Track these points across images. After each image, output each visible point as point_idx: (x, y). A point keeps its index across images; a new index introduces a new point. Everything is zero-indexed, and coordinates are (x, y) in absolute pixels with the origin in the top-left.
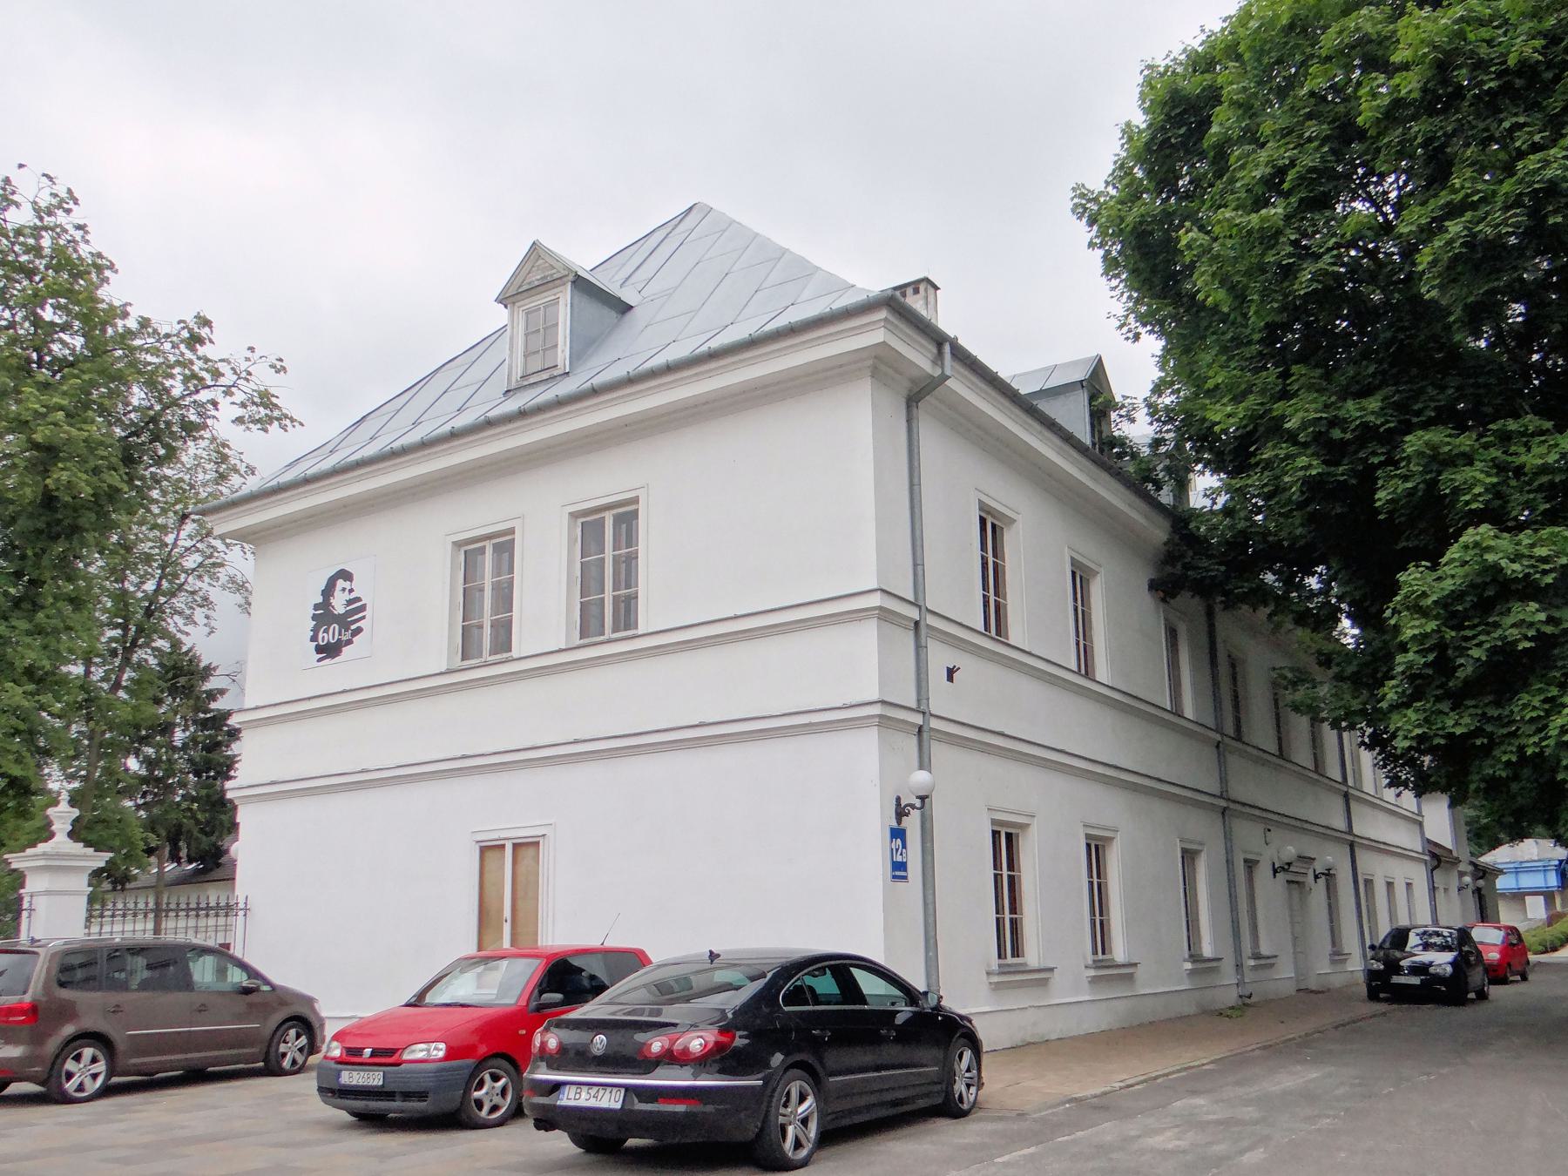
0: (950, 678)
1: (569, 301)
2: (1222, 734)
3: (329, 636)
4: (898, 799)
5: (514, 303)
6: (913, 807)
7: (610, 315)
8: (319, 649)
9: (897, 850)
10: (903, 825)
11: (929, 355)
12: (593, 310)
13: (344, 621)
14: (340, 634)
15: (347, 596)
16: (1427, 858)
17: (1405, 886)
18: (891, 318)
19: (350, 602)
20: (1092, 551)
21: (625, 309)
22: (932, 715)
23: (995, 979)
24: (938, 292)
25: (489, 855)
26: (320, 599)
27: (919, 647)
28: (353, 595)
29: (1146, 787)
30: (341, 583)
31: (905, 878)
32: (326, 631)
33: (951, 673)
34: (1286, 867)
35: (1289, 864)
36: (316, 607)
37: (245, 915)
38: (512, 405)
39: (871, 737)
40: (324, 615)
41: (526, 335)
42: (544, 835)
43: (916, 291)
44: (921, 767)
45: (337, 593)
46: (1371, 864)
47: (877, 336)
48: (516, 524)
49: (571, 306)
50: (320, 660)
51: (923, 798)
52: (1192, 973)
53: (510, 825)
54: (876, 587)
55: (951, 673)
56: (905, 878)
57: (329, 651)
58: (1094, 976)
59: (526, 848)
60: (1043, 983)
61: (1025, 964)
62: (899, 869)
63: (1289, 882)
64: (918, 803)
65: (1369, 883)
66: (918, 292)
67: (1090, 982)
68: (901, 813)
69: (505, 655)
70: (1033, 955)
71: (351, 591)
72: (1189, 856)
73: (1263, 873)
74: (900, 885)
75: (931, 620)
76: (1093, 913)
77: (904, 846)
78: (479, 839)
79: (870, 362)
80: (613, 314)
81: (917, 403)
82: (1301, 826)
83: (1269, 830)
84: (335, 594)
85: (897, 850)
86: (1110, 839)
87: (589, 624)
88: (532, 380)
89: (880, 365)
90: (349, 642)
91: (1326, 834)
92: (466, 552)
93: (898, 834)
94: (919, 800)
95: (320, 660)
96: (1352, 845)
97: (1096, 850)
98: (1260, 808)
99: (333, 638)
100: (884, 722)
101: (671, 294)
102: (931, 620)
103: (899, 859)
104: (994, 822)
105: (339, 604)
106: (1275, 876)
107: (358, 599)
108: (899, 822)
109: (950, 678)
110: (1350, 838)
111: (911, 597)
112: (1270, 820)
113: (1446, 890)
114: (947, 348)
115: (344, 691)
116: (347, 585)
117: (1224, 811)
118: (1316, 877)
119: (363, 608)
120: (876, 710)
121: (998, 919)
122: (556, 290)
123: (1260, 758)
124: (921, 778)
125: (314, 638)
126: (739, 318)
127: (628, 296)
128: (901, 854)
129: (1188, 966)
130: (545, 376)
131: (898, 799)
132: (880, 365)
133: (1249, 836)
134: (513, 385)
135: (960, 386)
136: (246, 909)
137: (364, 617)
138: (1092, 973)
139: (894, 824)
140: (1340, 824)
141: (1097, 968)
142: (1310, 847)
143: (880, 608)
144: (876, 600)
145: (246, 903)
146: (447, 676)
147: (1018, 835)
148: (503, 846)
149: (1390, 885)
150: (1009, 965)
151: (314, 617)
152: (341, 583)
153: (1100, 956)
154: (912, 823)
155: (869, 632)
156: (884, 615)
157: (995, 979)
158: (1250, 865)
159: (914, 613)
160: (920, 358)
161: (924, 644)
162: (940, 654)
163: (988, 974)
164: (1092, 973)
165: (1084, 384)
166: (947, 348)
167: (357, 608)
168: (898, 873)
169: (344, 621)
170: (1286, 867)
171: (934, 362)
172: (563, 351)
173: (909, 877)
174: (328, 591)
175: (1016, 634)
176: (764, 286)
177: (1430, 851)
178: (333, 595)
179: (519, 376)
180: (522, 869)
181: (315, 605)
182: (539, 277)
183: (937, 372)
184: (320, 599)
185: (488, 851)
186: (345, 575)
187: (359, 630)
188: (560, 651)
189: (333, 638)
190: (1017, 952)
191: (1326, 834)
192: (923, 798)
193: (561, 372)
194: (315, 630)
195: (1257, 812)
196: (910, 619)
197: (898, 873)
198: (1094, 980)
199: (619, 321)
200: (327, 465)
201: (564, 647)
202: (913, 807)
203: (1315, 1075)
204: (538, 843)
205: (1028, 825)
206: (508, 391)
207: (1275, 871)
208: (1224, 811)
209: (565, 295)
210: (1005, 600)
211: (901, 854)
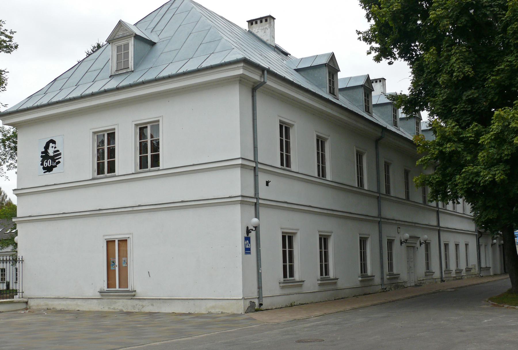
0: (267, 185)
1: (133, 44)
2: (380, 193)
3: (49, 163)
4: (248, 227)
5: (112, 42)
6: (252, 230)
7: (148, 47)
8: (44, 168)
9: (247, 244)
10: (249, 236)
11: (259, 75)
12: (142, 46)
13: (53, 158)
14: (52, 163)
15: (53, 149)
16: (476, 233)
17: (454, 246)
18: (245, 65)
19: (55, 152)
20: (324, 132)
21: (153, 44)
22: (260, 199)
23: (282, 285)
24: (275, 20)
25: (110, 244)
26: (44, 150)
27: (256, 176)
28: (56, 149)
29: (345, 216)
30: (51, 145)
31: (250, 253)
32: (47, 162)
33: (267, 183)
34: (405, 241)
35: (406, 240)
36: (42, 153)
37: (22, 263)
38: (113, 84)
39: (238, 207)
40: (45, 156)
41: (117, 63)
42: (129, 237)
43: (266, 21)
44: (256, 217)
45: (50, 148)
46: (445, 237)
47: (240, 72)
48: (116, 127)
49: (134, 46)
50: (44, 172)
51: (255, 227)
52: (361, 281)
53: (117, 234)
54: (239, 157)
55: (267, 183)
56: (250, 253)
57: (49, 169)
58: (320, 283)
59: (123, 242)
60: (301, 286)
61: (294, 280)
62: (247, 250)
63: (407, 246)
64: (254, 229)
65: (446, 245)
66: (267, 21)
67: (319, 285)
68: (248, 231)
69: (113, 174)
70: (297, 276)
71: (55, 147)
72: (363, 241)
73: (396, 246)
74: (248, 255)
75: (260, 166)
76: (321, 261)
77: (250, 243)
78: (106, 238)
79: (239, 79)
80: (149, 46)
81: (256, 90)
82: (414, 225)
83: (399, 228)
84: (49, 148)
85: (247, 244)
86: (329, 236)
87: (143, 164)
88: (120, 72)
89: (241, 80)
90: (56, 166)
91: (428, 228)
92: (97, 135)
93: (247, 239)
94: (254, 228)
95: (44, 172)
96: (439, 231)
97: (324, 240)
98: (395, 220)
99: (49, 165)
100: (242, 203)
101: (170, 40)
102: (260, 166)
103: (248, 247)
104: (283, 233)
105: (51, 152)
106: (401, 245)
107: (58, 151)
108: (248, 235)
109: (267, 185)
110: (438, 228)
111: (252, 159)
112: (399, 224)
113: (486, 246)
114: (266, 72)
115: (55, 184)
116: (54, 145)
117: (379, 222)
118: (421, 244)
119: (60, 154)
120: (240, 199)
121: (320, 251)
122: (128, 39)
123: (398, 201)
124: (255, 220)
125: (42, 164)
126: (195, 56)
127: (154, 39)
128: (248, 245)
129: (360, 279)
130: (124, 71)
131: (248, 227)
132: (241, 80)
133: (389, 232)
134: (113, 74)
135: (271, 83)
136: (22, 261)
137: (60, 158)
138: (319, 282)
139: (246, 235)
140: (435, 223)
141: (321, 280)
142: (418, 233)
143: (241, 164)
144: (240, 162)
145: (22, 259)
146: (92, 181)
147: (293, 236)
148: (114, 241)
149: (457, 245)
150: (288, 280)
151: (42, 157)
152: (51, 145)
153: (324, 276)
154: (253, 235)
155: (238, 172)
156: (242, 166)
157: (282, 285)
158: (390, 242)
159: (254, 165)
160: (256, 76)
161: (257, 175)
162: (262, 178)
163: (280, 283)
164: (319, 282)
165: (326, 65)
166: (266, 72)
167: (57, 154)
168: (247, 252)
169: (53, 158)
170: (405, 241)
171: (261, 77)
172: (131, 62)
173: (251, 253)
174: (47, 147)
175: (294, 167)
176: (203, 42)
177: (478, 231)
178: (48, 149)
179: (115, 70)
180: (122, 248)
181: (42, 152)
182: (121, 33)
183: (262, 80)
184: (44, 150)
185: (110, 243)
186: (53, 142)
187: (59, 162)
188: (133, 174)
189: (49, 165)
190: (292, 275)
191: (428, 228)
192: (255, 227)
193: (130, 70)
194: (42, 162)
195: (394, 222)
196: (253, 166)
197: (247, 252)
198: (320, 285)
199: (151, 49)
200: (45, 101)
201: (134, 172)
202: (252, 230)
203: (23, 312)
204: (127, 240)
205: (296, 233)
206: (111, 76)
207: (401, 243)
208: (379, 222)
209: (131, 42)
210: (290, 153)
211: (248, 245)
